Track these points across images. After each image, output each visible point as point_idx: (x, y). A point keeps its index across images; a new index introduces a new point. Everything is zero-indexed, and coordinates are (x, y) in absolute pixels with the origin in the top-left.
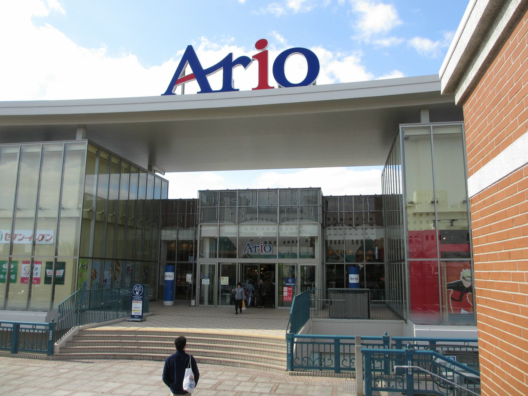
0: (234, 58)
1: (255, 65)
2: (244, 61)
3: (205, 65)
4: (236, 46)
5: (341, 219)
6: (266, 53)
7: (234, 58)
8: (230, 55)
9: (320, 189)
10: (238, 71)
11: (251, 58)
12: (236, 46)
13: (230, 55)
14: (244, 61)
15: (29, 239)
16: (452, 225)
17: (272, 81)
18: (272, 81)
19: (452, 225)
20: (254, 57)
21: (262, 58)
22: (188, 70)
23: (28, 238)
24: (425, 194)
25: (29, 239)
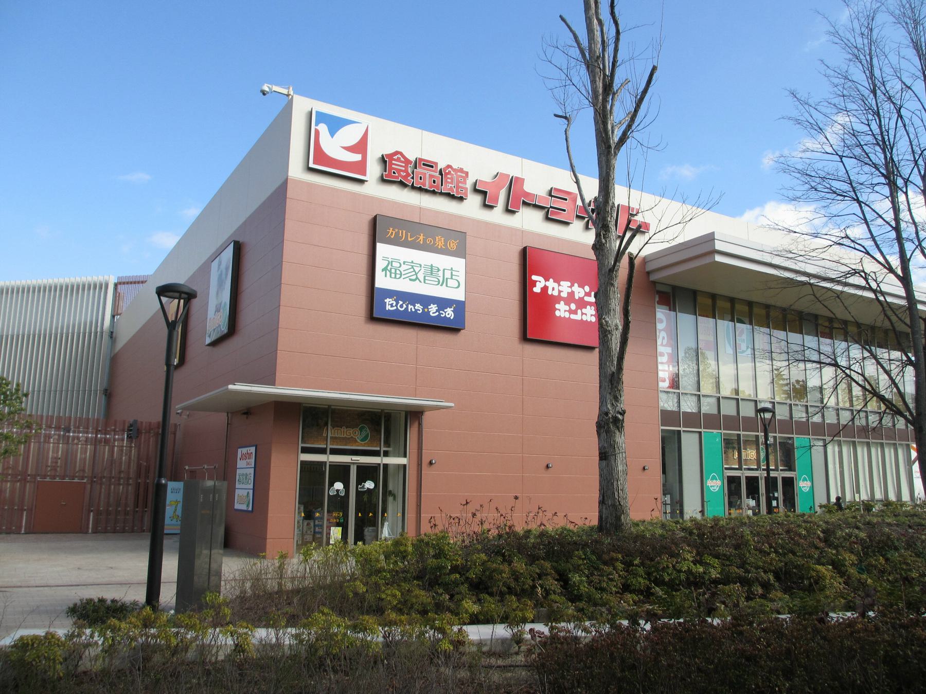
9: (524, 179)
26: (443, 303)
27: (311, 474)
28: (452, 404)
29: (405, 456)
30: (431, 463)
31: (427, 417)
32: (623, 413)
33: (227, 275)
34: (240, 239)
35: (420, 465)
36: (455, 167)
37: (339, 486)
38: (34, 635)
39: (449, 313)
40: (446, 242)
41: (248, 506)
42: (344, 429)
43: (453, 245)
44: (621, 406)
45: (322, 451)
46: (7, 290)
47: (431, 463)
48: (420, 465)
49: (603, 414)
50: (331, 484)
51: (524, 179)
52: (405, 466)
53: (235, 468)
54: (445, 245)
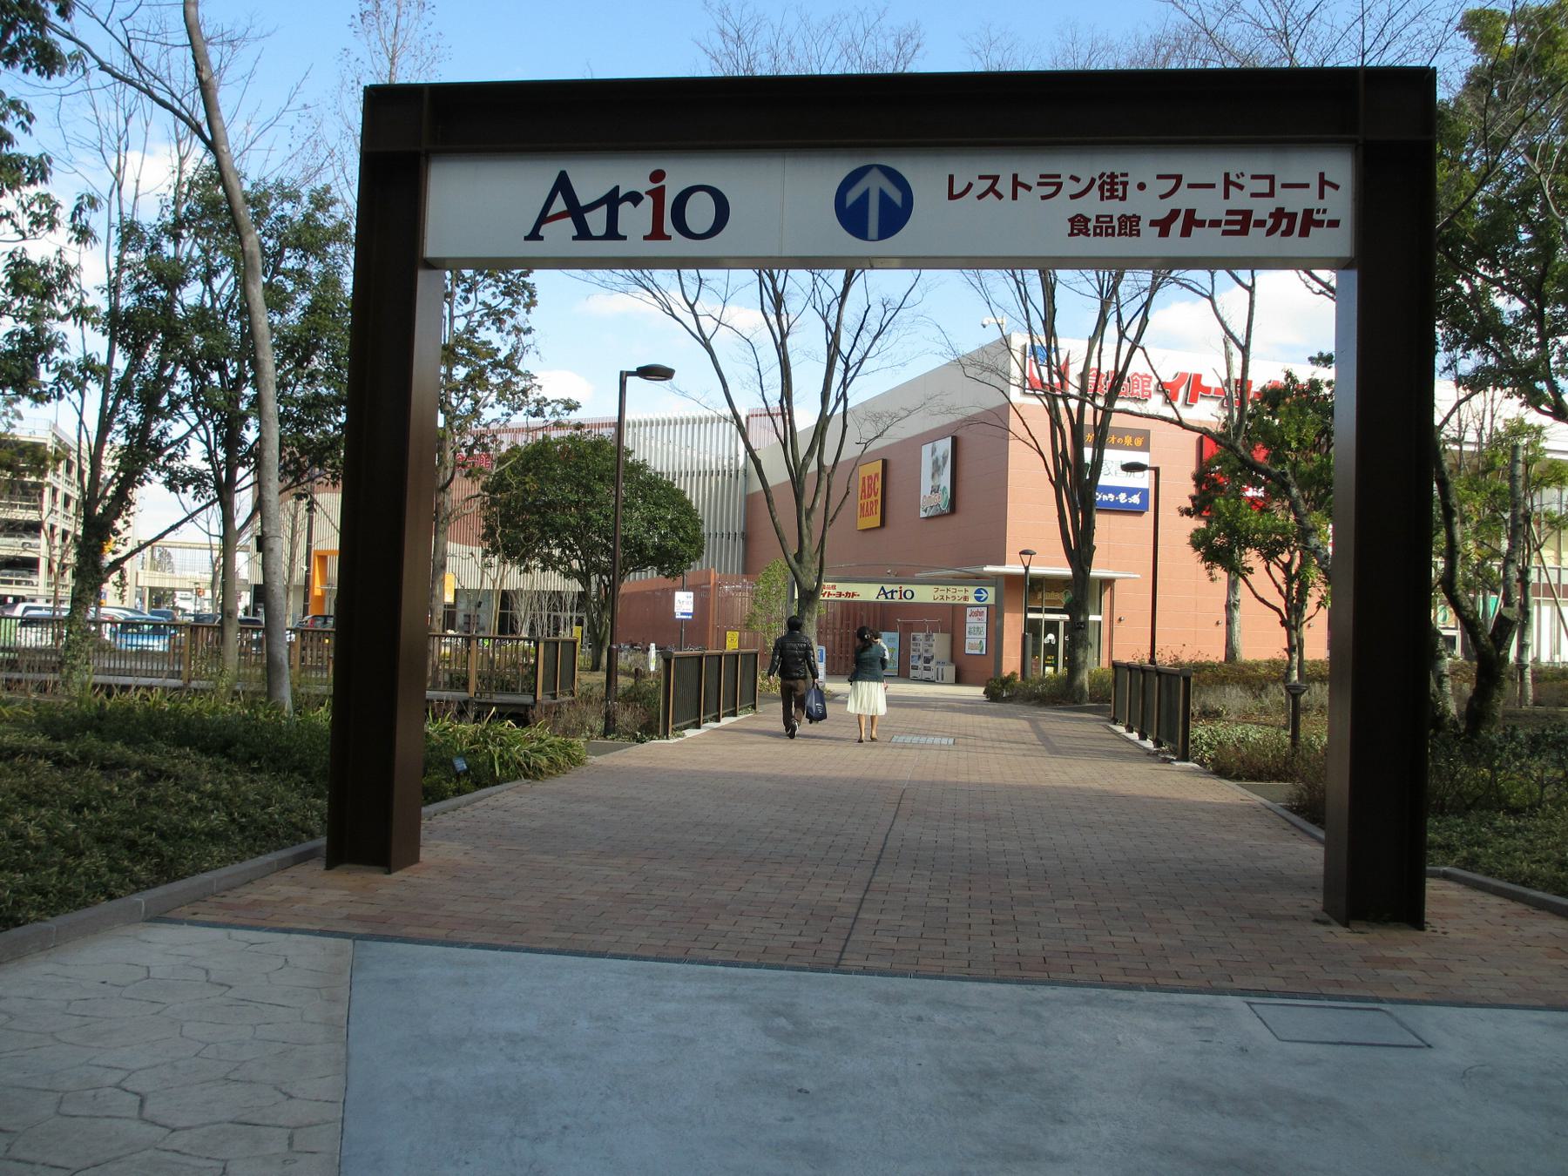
0: (621, 193)
1: (648, 202)
2: (635, 198)
3: (584, 200)
4: (1286, 211)
5: (178, 675)
6: (662, 188)
7: (621, 193)
8: (617, 188)
9: (1247, 234)
10: (625, 208)
11: (643, 194)
12: (1286, 211)
13: (617, 188)
14: (635, 198)
15: (1157, 229)
16: (1334, 224)
17: (668, 227)
18: (668, 227)
19: (1334, 224)
20: (647, 193)
21: (658, 195)
22: (559, 205)
23: (1201, 224)
24: (1173, 1043)
25: (1157, 229)
26: (1130, 492)
27: (1032, 628)
28: (1138, 576)
29: (1100, 614)
30: (1120, 620)
31: (1116, 585)
32: (1239, 601)
33: (944, 464)
34: (958, 434)
35: (1111, 621)
36: (1140, 374)
37: (1051, 636)
38: (10, 134)
39: (1135, 499)
40: (1133, 440)
41: (981, 650)
42: (1053, 594)
43: (1139, 442)
44: (1238, 597)
45: (1039, 611)
46: (694, 421)
47: (1120, 620)
48: (1111, 621)
49: (1228, 601)
50: (1045, 636)
51: (1247, 234)
52: (1100, 622)
53: (965, 623)
54: (1133, 442)
